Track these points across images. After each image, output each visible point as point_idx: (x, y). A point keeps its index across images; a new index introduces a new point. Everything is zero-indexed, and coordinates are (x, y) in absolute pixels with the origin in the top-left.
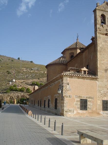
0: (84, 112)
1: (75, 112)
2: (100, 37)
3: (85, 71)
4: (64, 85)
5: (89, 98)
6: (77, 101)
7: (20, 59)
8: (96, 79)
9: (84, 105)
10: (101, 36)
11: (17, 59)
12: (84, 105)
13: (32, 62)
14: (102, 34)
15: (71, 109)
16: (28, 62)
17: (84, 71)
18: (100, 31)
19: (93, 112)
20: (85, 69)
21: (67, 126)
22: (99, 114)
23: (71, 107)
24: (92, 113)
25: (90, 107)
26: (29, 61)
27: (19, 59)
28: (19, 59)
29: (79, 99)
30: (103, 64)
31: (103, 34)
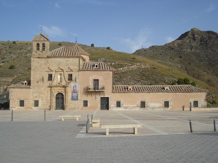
0: (22, 107)
1: (16, 108)
2: (34, 60)
3: (26, 83)
4: (10, 93)
5: (26, 99)
6: (18, 102)
7: (95, 46)
8: (30, 88)
9: (22, 103)
10: (35, 59)
11: (91, 46)
12: (22, 103)
13: (108, 48)
14: (36, 58)
15: (14, 106)
16: (103, 49)
17: (25, 83)
18: (34, 56)
19: (28, 108)
20: (26, 82)
21: (150, 135)
22: (31, 108)
23: (14, 105)
24: (27, 108)
25: (26, 105)
26: (105, 48)
27: (92, 45)
28: (92, 45)
29: (19, 101)
30: (35, 78)
31: (37, 58)
